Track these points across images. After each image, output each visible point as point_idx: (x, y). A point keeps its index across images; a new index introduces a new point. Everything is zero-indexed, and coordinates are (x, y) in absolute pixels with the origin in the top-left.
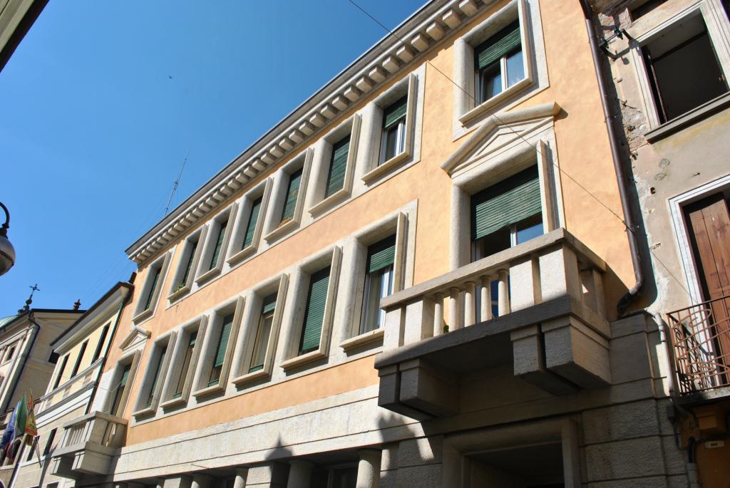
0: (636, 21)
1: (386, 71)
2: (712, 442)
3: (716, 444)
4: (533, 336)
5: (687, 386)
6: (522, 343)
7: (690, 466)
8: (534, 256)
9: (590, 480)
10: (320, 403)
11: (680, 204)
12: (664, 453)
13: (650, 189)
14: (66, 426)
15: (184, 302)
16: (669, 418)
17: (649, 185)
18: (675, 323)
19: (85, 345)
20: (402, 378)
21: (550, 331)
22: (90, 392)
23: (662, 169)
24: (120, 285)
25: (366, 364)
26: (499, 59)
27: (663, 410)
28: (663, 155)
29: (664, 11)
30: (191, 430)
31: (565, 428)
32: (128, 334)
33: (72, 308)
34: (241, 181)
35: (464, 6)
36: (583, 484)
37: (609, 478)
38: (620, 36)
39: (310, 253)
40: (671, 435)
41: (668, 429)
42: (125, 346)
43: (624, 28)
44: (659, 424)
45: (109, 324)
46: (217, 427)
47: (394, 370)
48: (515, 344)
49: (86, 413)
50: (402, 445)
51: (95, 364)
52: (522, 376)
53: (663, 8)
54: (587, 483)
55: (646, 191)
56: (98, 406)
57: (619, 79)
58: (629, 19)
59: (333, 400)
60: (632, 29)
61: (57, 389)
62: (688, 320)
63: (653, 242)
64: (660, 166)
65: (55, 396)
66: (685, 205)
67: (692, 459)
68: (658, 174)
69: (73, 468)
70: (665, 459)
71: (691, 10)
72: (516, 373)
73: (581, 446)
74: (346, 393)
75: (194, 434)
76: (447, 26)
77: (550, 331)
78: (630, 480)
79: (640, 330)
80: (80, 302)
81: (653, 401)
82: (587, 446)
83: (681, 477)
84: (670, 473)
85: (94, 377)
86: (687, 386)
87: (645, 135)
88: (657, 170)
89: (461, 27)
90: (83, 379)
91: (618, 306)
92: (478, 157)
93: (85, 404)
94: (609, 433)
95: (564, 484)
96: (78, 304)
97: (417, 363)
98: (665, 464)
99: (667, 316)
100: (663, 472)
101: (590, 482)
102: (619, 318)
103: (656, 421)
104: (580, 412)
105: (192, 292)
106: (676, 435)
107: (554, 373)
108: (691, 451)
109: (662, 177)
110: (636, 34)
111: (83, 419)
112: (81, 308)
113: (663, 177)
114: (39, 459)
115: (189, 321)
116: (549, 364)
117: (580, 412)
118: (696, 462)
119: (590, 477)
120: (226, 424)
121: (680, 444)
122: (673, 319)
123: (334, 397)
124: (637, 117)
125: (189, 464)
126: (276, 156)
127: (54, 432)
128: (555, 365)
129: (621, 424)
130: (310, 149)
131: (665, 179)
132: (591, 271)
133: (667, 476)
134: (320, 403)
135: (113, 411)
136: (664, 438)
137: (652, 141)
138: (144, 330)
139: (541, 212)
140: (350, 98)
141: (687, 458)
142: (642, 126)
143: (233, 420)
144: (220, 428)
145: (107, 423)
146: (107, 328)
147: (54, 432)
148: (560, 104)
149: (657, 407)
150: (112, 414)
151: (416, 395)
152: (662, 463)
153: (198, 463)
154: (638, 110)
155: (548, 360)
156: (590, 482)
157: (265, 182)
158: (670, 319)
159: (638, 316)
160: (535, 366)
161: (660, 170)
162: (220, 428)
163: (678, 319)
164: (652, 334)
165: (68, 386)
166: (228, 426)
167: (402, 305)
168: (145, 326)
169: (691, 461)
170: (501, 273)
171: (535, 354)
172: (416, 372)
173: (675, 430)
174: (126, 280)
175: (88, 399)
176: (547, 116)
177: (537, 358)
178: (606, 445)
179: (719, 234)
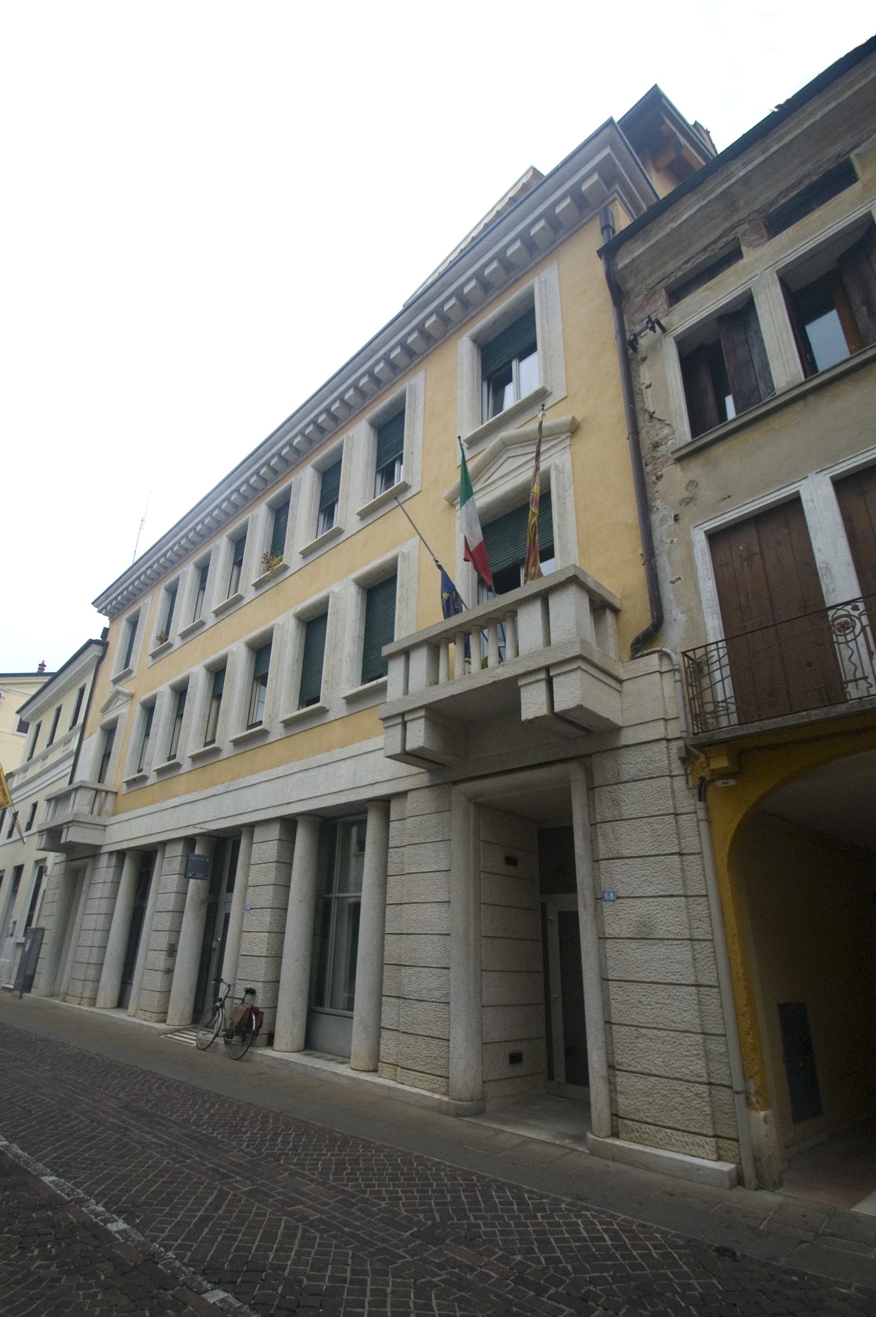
0: (673, 307)
1: (379, 379)
2: (722, 781)
3: (727, 783)
4: (541, 680)
5: (699, 726)
6: (530, 687)
7: (700, 805)
8: (544, 597)
9: (598, 821)
10: (324, 758)
11: (706, 532)
12: (673, 792)
13: (673, 516)
14: (48, 798)
15: (166, 661)
16: (680, 758)
17: (672, 512)
18: (690, 662)
19: (59, 710)
20: (408, 728)
21: (559, 675)
22: (71, 761)
23: (688, 493)
24: (91, 642)
25: (370, 718)
26: (510, 362)
27: (674, 752)
28: (691, 476)
29: (709, 292)
30: (191, 792)
31: (575, 773)
32: (108, 696)
33: (35, 670)
34: (186, 546)
35: (470, 291)
36: (592, 825)
37: (618, 818)
38: (653, 329)
39: (304, 600)
40: (682, 775)
41: (677, 768)
42: (105, 709)
43: (659, 316)
44: (670, 764)
45: (84, 686)
46: (217, 787)
47: (399, 720)
48: (522, 690)
49: (71, 782)
50: (410, 795)
51: (72, 731)
52: (530, 721)
53: (707, 289)
54: (596, 824)
55: (669, 519)
56: (86, 773)
57: (648, 383)
58: (665, 306)
59: (337, 754)
60: (668, 318)
61: (31, 761)
62: (705, 658)
63: (672, 575)
64: (687, 490)
65: (30, 769)
66: (711, 533)
67: (702, 796)
68: (684, 499)
69: (63, 841)
70: (674, 799)
71: (740, 291)
72: (523, 719)
73: (591, 788)
74: (351, 746)
75: (193, 797)
76: (450, 319)
77: (559, 675)
78: (638, 820)
79: (653, 670)
80: (45, 663)
81: (664, 742)
82: (596, 788)
83: (690, 815)
84: (679, 812)
85: (74, 745)
86: (699, 726)
87: (672, 453)
88: (682, 493)
89: (466, 320)
90: (62, 748)
91: (632, 646)
92: (483, 485)
93: (68, 774)
94: (619, 774)
95: (572, 826)
96: (42, 666)
97: (422, 713)
98: (674, 803)
99: (681, 655)
100: (672, 811)
101: (599, 823)
102: (633, 658)
103: (666, 762)
104: (590, 755)
105: (271, 739)
106: (686, 775)
107: (562, 717)
108: (702, 790)
109: (687, 501)
110: (672, 325)
111: (67, 790)
112: (47, 670)
113: (689, 502)
114: (21, 836)
115: (178, 678)
116: (557, 709)
117: (590, 755)
118: (705, 801)
119: (599, 818)
120: (226, 784)
121: (690, 784)
122: (688, 657)
123: (339, 750)
124: (666, 431)
125: (191, 827)
126: (257, 487)
127: (35, 806)
128: (563, 709)
129: (631, 766)
130: (347, 436)
131: (691, 504)
132: (604, 610)
133: (676, 815)
134: (324, 758)
135: (101, 779)
136: (674, 778)
137: (679, 460)
138: (127, 691)
139: (553, 545)
140: (415, 349)
141: (697, 797)
142: (670, 442)
143: (234, 779)
144: (220, 788)
145: (95, 792)
146: (82, 691)
147: (35, 806)
148: (579, 419)
149: (667, 748)
150: (99, 782)
151: (422, 745)
152: (671, 803)
153: (199, 826)
154: (667, 422)
155: (555, 704)
156: (599, 823)
157: (248, 519)
158: (686, 658)
159: (652, 655)
160: (543, 711)
161: (686, 494)
162: (220, 788)
163: (693, 657)
164: (666, 674)
165: (44, 757)
166: (229, 785)
167: (406, 653)
168: (126, 687)
169: (700, 800)
170: (510, 613)
171: (543, 698)
172: (422, 721)
173: (686, 770)
174: (98, 636)
175: (70, 770)
176: (562, 433)
177: (545, 702)
178: (616, 787)
179: (745, 565)
